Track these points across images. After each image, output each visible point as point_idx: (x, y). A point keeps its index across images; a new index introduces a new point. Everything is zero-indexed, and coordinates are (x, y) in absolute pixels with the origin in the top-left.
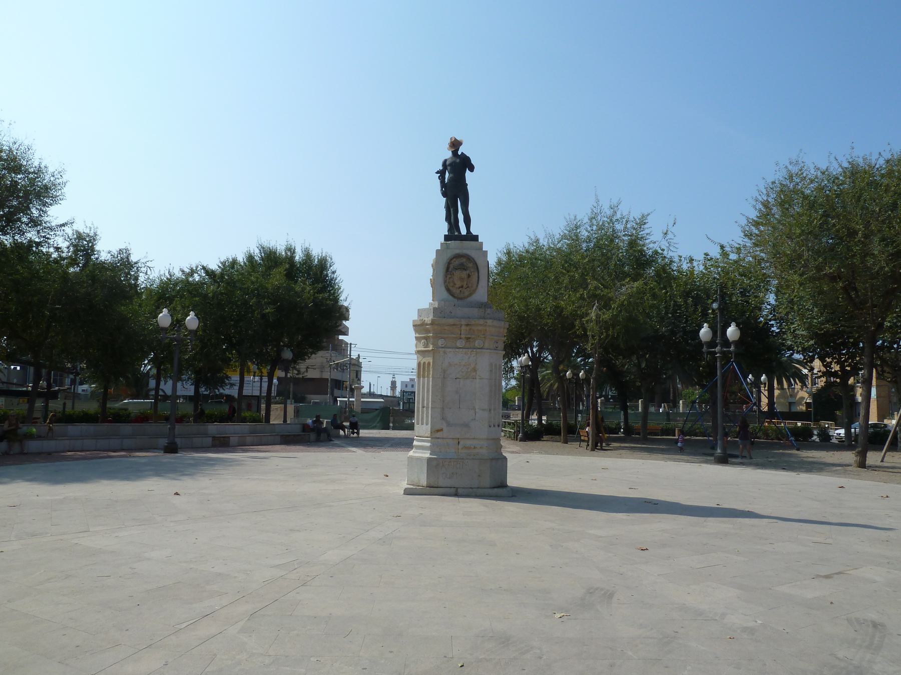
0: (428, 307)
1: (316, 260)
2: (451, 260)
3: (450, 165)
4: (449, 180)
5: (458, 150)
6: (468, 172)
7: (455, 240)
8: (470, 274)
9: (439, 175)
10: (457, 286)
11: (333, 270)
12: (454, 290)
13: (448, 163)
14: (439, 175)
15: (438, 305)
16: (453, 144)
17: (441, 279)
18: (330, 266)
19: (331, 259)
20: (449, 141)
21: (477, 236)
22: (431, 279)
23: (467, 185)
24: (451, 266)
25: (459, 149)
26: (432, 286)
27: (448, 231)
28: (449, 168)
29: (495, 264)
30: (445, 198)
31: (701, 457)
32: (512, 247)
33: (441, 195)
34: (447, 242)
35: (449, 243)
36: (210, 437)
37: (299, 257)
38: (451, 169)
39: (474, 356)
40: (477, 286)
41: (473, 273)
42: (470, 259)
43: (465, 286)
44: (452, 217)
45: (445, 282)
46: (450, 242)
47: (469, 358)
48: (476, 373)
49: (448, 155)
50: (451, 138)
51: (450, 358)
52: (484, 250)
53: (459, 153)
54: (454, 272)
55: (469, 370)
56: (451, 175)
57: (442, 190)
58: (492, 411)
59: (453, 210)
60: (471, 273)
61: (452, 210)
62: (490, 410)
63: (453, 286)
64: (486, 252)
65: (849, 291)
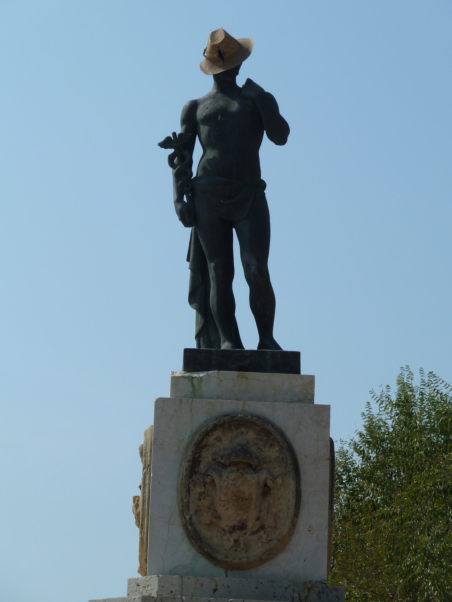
0: (125, 595)
2: (207, 433)
3: (208, 119)
4: (203, 168)
5: (236, 71)
7: (220, 367)
8: (269, 482)
9: (171, 151)
10: (225, 524)
13: (201, 113)
14: (171, 151)
15: (161, 586)
16: (221, 55)
20: (206, 43)
21: (296, 356)
22: (136, 499)
23: (263, 185)
25: (238, 67)
26: (140, 523)
27: (198, 337)
28: (204, 129)
29: (357, 439)
30: (189, 230)
31: (215, 303)
32: (416, 383)
33: (177, 218)
34: (195, 375)
35: (201, 379)
38: (209, 134)
40: (294, 525)
41: (279, 480)
42: (268, 433)
43: (251, 524)
44: (213, 292)
46: (202, 375)
50: (213, 35)
52: (317, 401)
53: (240, 81)
54: (214, 475)
56: (211, 154)
57: (179, 200)
59: (215, 268)
60: (274, 479)
61: (211, 266)
63: (210, 525)
64: (326, 409)
65: (239, 434)
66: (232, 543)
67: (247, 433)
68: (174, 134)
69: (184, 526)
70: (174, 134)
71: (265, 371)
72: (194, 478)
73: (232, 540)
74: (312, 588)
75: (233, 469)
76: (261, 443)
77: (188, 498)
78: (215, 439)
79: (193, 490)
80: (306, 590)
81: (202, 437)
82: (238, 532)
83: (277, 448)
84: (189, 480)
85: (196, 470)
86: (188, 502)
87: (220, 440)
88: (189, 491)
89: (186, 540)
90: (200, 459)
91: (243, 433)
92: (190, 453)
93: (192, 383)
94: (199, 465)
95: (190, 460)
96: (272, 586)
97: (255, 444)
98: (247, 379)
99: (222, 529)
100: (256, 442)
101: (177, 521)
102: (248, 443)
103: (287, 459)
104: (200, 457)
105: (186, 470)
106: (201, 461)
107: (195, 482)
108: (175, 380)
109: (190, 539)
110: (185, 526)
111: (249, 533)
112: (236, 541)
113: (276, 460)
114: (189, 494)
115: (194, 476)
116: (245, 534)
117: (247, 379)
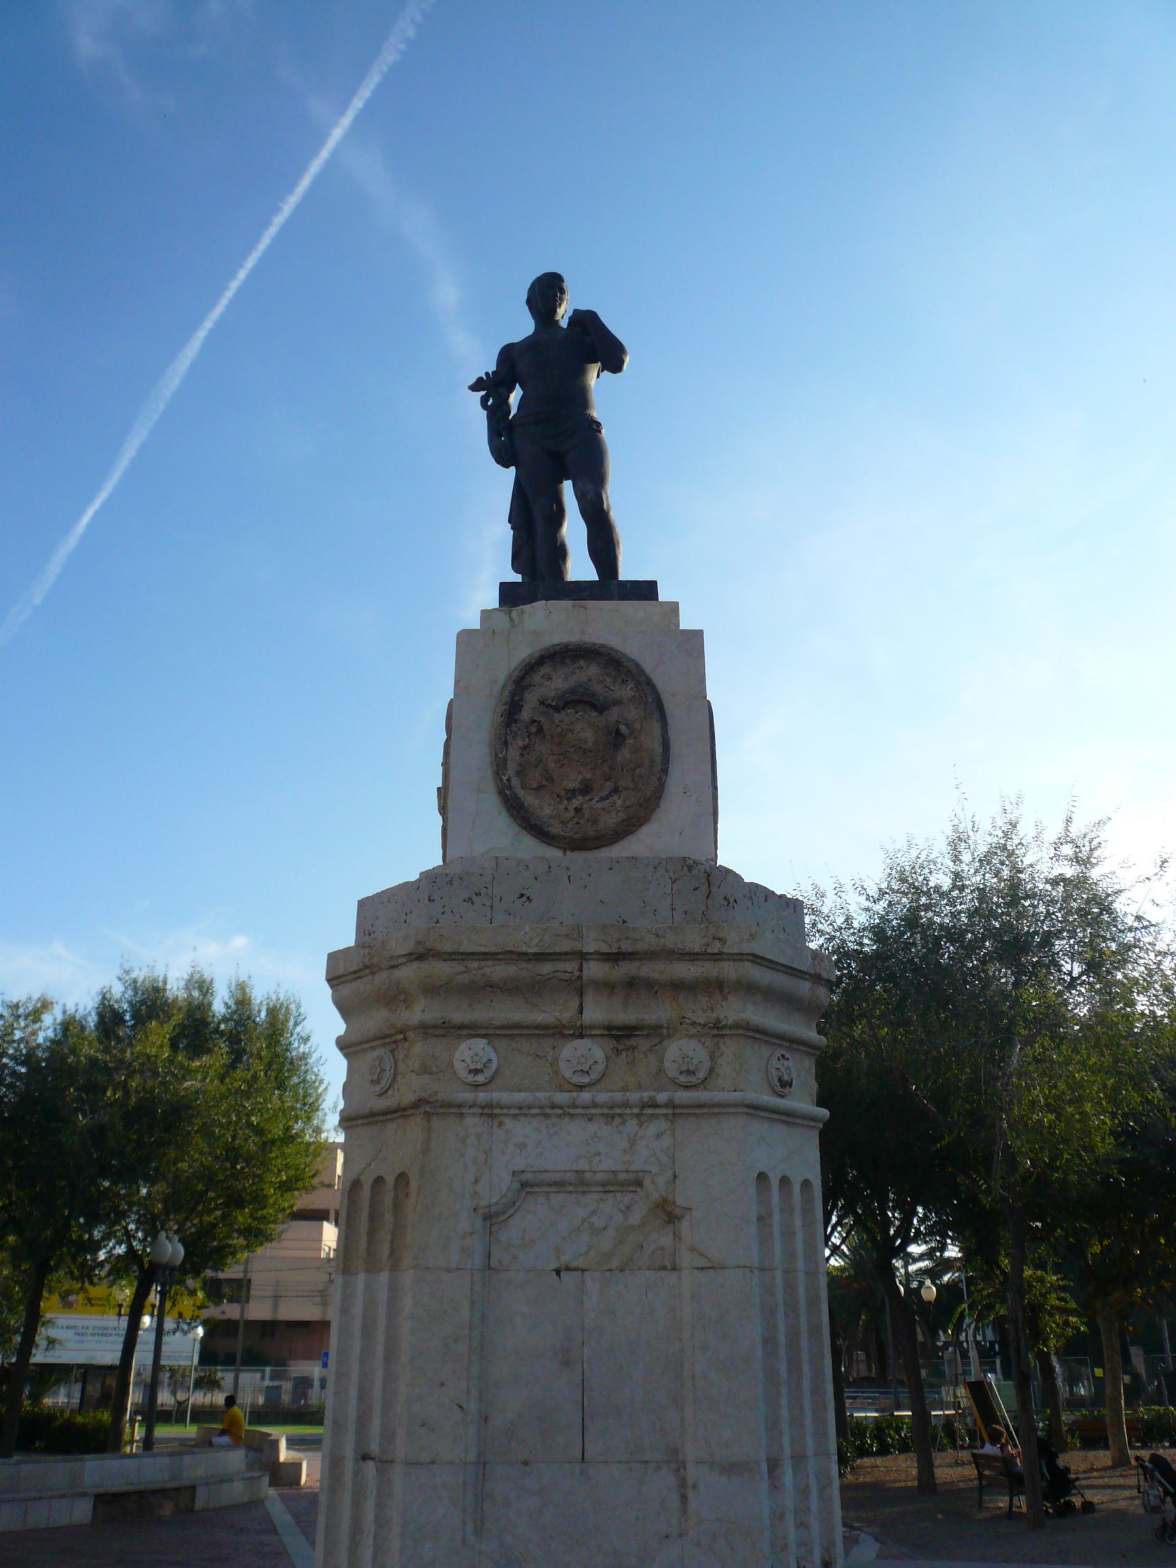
1: (263, 1014)
6: (596, 380)
9: (483, 393)
11: (303, 1034)
12: (543, 808)
14: (483, 393)
17: (478, 755)
18: (296, 1024)
19: (298, 1007)
22: (439, 789)
23: (595, 427)
24: (531, 700)
36: (84, 1495)
37: (219, 1005)
39: (658, 1136)
45: (499, 765)
47: (633, 1142)
48: (677, 1236)
49: (523, 326)
51: (522, 1146)
55: (635, 1219)
58: (787, 1476)
62: (774, 1465)
66: (572, 813)
67: (588, 667)
68: (487, 374)
69: (500, 793)
70: (487, 374)
71: (611, 599)
72: (514, 728)
73: (571, 808)
74: (695, 866)
75: (569, 711)
76: (609, 680)
77: (504, 752)
78: (542, 677)
79: (512, 744)
80: (686, 869)
81: (523, 672)
82: (580, 798)
83: (631, 685)
84: (506, 730)
85: (516, 717)
86: (505, 759)
87: (551, 679)
88: (506, 743)
89: (504, 813)
90: (521, 703)
91: (582, 668)
92: (507, 693)
93: (510, 617)
94: (521, 711)
95: (507, 703)
96: (634, 865)
97: (601, 682)
98: (586, 609)
99: (556, 796)
100: (601, 679)
101: (490, 787)
102: (590, 680)
103: (646, 696)
104: (521, 699)
105: (501, 716)
106: (523, 706)
107: (515, 733)
108: (486, 614)
109: (508, 810)
110: (501, 792)
111: (596, 799)
112: (577, 810)
113: (631, 701)
114: (506, 749)
115: (514, 725)
116: (591, 800)
117: (586, 609)
